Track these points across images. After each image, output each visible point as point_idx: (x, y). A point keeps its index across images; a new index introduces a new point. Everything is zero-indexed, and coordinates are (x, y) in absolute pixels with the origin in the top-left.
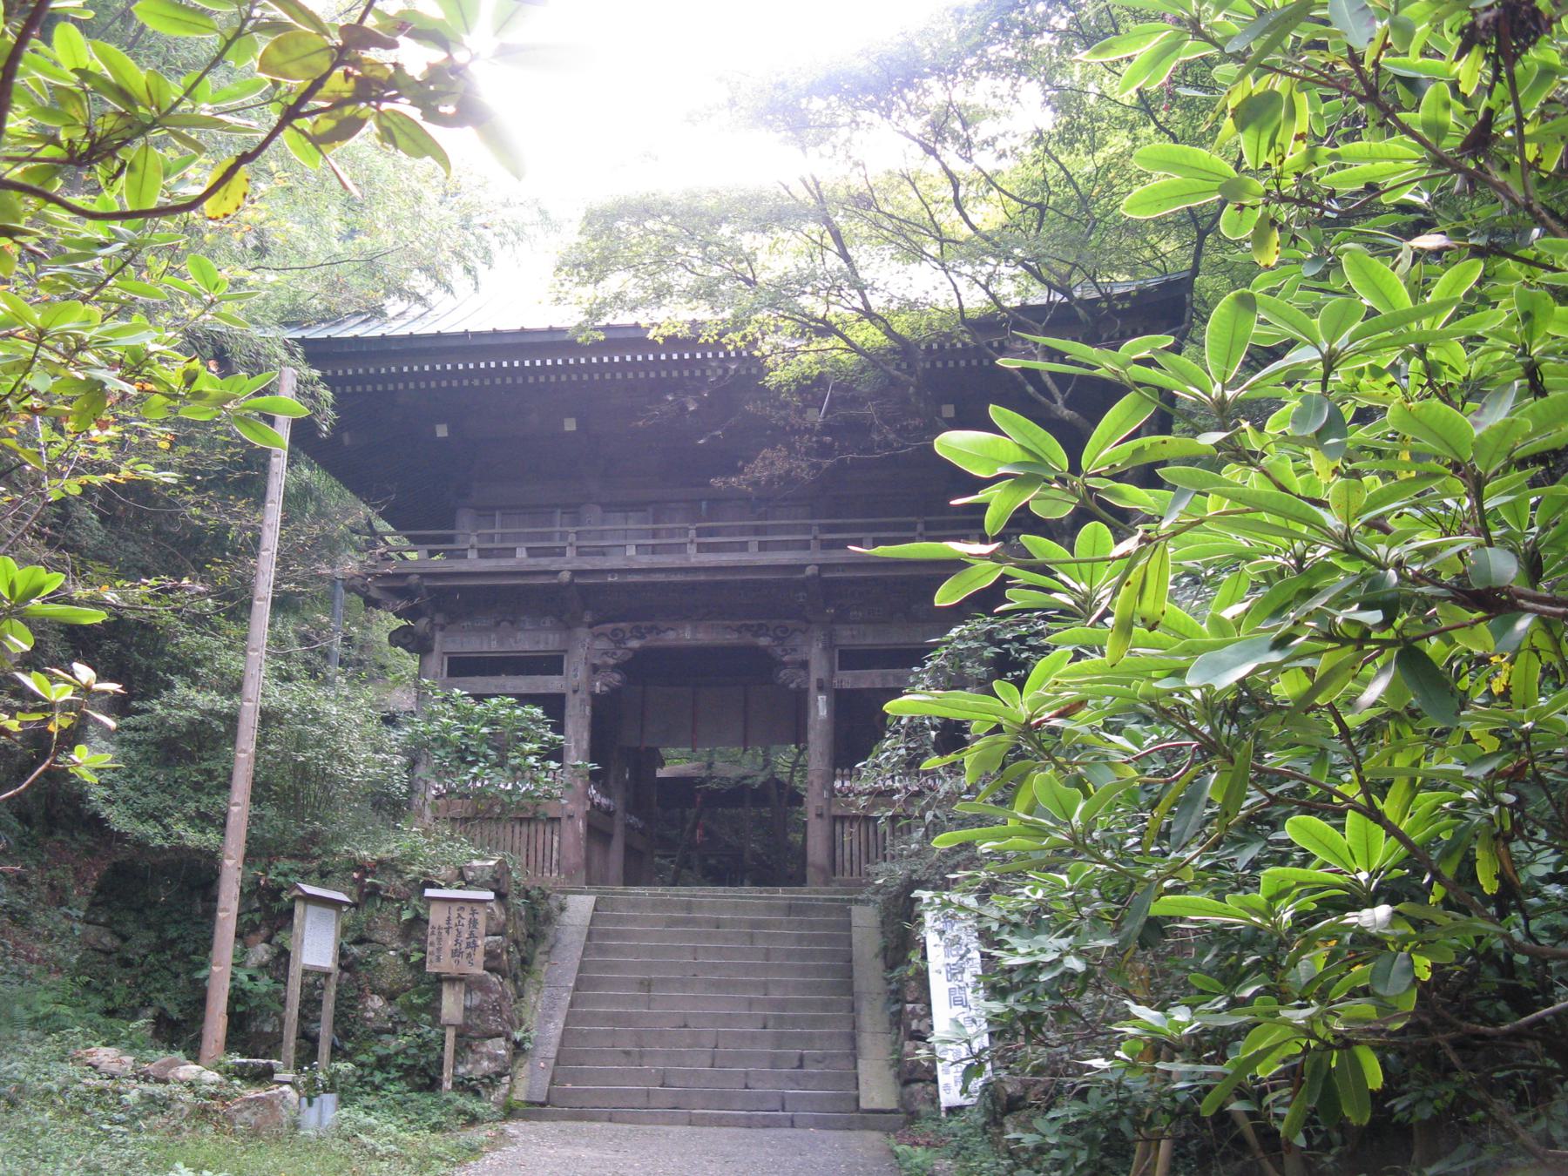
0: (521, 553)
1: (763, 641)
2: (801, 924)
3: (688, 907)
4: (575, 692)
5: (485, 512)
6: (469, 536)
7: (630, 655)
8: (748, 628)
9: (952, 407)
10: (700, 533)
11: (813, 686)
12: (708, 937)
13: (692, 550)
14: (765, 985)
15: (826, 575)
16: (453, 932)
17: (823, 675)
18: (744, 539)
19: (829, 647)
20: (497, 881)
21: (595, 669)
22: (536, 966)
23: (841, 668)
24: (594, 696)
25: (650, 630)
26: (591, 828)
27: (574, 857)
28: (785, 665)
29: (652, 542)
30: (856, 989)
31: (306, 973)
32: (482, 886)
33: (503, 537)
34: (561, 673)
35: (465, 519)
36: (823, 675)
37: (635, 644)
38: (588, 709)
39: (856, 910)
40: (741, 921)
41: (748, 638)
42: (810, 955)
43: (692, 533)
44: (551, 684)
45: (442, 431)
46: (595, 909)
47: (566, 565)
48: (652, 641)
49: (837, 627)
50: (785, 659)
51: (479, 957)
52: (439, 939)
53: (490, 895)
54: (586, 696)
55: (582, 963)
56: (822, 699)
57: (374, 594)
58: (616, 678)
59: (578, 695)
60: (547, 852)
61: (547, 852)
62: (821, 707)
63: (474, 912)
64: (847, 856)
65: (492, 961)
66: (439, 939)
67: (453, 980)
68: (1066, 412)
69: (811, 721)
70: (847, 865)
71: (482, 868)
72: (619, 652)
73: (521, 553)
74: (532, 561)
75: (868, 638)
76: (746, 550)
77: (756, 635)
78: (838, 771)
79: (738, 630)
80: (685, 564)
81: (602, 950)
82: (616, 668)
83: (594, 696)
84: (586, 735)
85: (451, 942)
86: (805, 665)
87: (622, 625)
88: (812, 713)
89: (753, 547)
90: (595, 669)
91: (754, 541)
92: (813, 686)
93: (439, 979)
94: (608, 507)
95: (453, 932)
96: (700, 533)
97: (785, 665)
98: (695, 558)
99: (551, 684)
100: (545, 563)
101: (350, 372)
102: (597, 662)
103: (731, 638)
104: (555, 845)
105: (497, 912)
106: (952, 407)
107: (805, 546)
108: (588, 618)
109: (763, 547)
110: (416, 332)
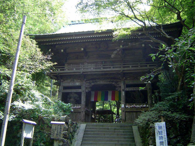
0: (75, 69)
1: (113, 83)
2: (123, 129)
3: (103, 126)
4: (83, 91)
5: (69, 64)
6: (66, 67)
7: (92, 86)
8: (111, 81)
9: (144, 45)
10: (103, 66)
11: (122, 90)
12: (106, 131)
13: (102, 68)
14: (118, 141)
15: (124, 72)
16: (57, 130)
17: (123, 88)
18: (110, 66)
19: (124, 84)
20: (66, 120)
21: (86, 88)
22: (75, 137)
23: (126, 87)
24: (86, 92)
25: (95, 81)
26: (85, 114)
27: (83, 118)
28: (117, 87)
29: (95, 67)
30: (135, 141)
31: (25, 138)
32: (63, 121)
33: (72, 67)
34: (81, 89)
35: (66, 65)
36: (123, 88)
37: (93, 84)
38: (85, 94)
39: (133, 127)
40: (112, 128)
41: (111, 83)
42: (126, 135)
43: (102, 66)
44: (79, 90)
45: (62, 51)
46: (86, 126)
47: (82, 71)
48: (95, 83)
49: (125, 81)
50: (117, 86)
51: (62, 136)
52: (54, 132)
53: (64, 123)
54: (85, 92)
55: (83, 136)
56: (123, 92)
57: (51, 76)
58: (90, 90)
59: (84, 92)
60: (79, 118)
61: (79, 118)
62: (123, 94)
63: (61, 126)
64: (128, 118)
65: (65, 136)
66: (54, 132)
67: (56, 140)
68: (169, 37)
69: (122, 96)
70: (128, 119)
71: (63, 118)
72: (90, 85)
73: (75, 69)
74: (76, 71)
75: (130, 82)
76: (111, 68)
77: (112, 82)
78: (126, 104)
79: (110, 81)
80: (101, 70)
81: (87, 134)
82: (90, 88)
83: (86, 92)
84: (85, 99)
85: (56, 132)
86: (120, 87)
87: (91, 81)
88: (122, 94)
89: (112, 68)
90: (86, 88)
91: (112, 67)
92: (122, 90)
93: (53, 140)
94: (88, 63)
95: (57, 130)
96: (103, 66)
97: (117, 87)
98: (102, 69)
99: (79, 90)
100: (78, 71)
101: (49, 44)
102: (86, 87)
103: (108, 83)
104: (80, 116)
105: (66, 126)
106: (144, 45)
107: (120, 67)
108: (85, 80)
109: (113, 68)
110: (58, 33)
